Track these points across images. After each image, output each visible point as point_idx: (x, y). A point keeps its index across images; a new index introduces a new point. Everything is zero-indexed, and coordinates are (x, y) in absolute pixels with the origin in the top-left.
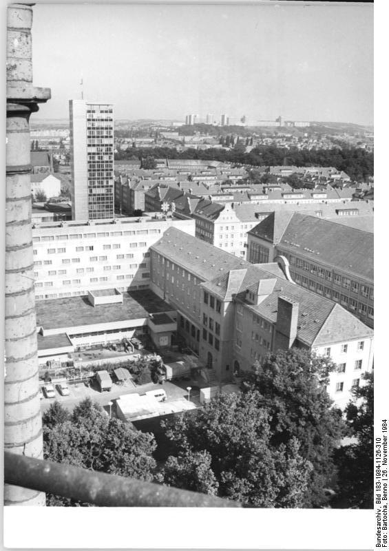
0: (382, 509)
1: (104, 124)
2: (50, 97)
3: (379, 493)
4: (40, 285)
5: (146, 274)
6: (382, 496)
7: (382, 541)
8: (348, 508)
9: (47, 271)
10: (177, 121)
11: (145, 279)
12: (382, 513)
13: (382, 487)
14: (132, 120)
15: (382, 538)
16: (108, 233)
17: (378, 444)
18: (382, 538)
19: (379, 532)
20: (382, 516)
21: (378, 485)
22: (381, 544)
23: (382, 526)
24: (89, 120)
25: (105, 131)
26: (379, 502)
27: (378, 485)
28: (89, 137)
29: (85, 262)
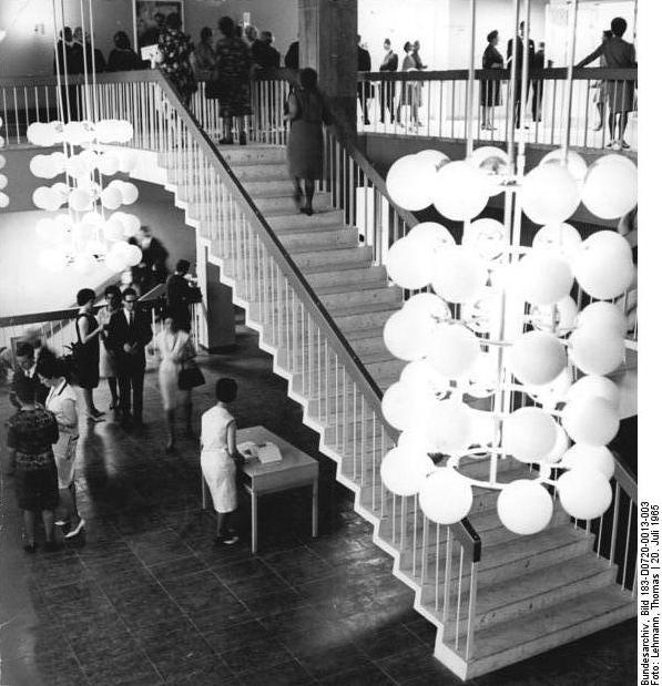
3: (645, 598)
7: (651, 676)
18: (651, 670)
19: (646, 661)
21: (645, 585)
26: (645, 613)
27: (645, 585)
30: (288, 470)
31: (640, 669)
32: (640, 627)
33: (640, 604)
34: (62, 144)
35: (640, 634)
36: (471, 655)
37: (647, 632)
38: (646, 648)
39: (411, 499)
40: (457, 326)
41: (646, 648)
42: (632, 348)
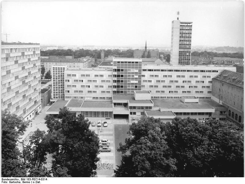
0: (19, 181)
1: (187, 32)
2: (243, 2)
3: (26, 179)
4: (179, 76)
5: (209, 92)
6: (24, 181)
7: (4, 181)
8: (212, 176)
9: (87, 80)
10: (159, 48)
11: (209, 94)
12: (17, 181)
13: (29, 181)
14: (52, 49)
15: (6, 181)
16: (180, 76)
17: (44, 179)
18: (6, 181)
19: (9, 179)
20: (16, 181)
21: (29, 179)
22: (3, 180)
23: (11, 181)
24: (181, 29)
25: (183, 36)
26: (22, 179)
27: (29, 179)
28: (180, 37)
29: (92, 85)
30: (235, 110)
31: (6, 178)
32: (18, 178)
33: (24, 178)
34: (122, 103)
35: (16, 178)
36: (164, 63)
37: (16, 180)
38: (12, 180)
39: (205, 51)
40: (108, 126)
41: (12, 180)
42: (144, 58)
